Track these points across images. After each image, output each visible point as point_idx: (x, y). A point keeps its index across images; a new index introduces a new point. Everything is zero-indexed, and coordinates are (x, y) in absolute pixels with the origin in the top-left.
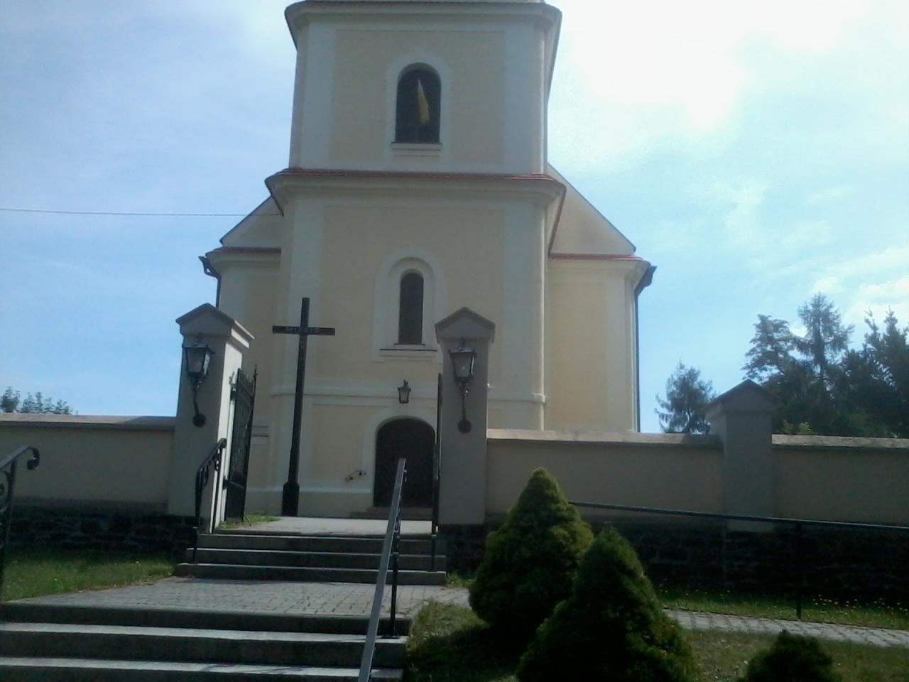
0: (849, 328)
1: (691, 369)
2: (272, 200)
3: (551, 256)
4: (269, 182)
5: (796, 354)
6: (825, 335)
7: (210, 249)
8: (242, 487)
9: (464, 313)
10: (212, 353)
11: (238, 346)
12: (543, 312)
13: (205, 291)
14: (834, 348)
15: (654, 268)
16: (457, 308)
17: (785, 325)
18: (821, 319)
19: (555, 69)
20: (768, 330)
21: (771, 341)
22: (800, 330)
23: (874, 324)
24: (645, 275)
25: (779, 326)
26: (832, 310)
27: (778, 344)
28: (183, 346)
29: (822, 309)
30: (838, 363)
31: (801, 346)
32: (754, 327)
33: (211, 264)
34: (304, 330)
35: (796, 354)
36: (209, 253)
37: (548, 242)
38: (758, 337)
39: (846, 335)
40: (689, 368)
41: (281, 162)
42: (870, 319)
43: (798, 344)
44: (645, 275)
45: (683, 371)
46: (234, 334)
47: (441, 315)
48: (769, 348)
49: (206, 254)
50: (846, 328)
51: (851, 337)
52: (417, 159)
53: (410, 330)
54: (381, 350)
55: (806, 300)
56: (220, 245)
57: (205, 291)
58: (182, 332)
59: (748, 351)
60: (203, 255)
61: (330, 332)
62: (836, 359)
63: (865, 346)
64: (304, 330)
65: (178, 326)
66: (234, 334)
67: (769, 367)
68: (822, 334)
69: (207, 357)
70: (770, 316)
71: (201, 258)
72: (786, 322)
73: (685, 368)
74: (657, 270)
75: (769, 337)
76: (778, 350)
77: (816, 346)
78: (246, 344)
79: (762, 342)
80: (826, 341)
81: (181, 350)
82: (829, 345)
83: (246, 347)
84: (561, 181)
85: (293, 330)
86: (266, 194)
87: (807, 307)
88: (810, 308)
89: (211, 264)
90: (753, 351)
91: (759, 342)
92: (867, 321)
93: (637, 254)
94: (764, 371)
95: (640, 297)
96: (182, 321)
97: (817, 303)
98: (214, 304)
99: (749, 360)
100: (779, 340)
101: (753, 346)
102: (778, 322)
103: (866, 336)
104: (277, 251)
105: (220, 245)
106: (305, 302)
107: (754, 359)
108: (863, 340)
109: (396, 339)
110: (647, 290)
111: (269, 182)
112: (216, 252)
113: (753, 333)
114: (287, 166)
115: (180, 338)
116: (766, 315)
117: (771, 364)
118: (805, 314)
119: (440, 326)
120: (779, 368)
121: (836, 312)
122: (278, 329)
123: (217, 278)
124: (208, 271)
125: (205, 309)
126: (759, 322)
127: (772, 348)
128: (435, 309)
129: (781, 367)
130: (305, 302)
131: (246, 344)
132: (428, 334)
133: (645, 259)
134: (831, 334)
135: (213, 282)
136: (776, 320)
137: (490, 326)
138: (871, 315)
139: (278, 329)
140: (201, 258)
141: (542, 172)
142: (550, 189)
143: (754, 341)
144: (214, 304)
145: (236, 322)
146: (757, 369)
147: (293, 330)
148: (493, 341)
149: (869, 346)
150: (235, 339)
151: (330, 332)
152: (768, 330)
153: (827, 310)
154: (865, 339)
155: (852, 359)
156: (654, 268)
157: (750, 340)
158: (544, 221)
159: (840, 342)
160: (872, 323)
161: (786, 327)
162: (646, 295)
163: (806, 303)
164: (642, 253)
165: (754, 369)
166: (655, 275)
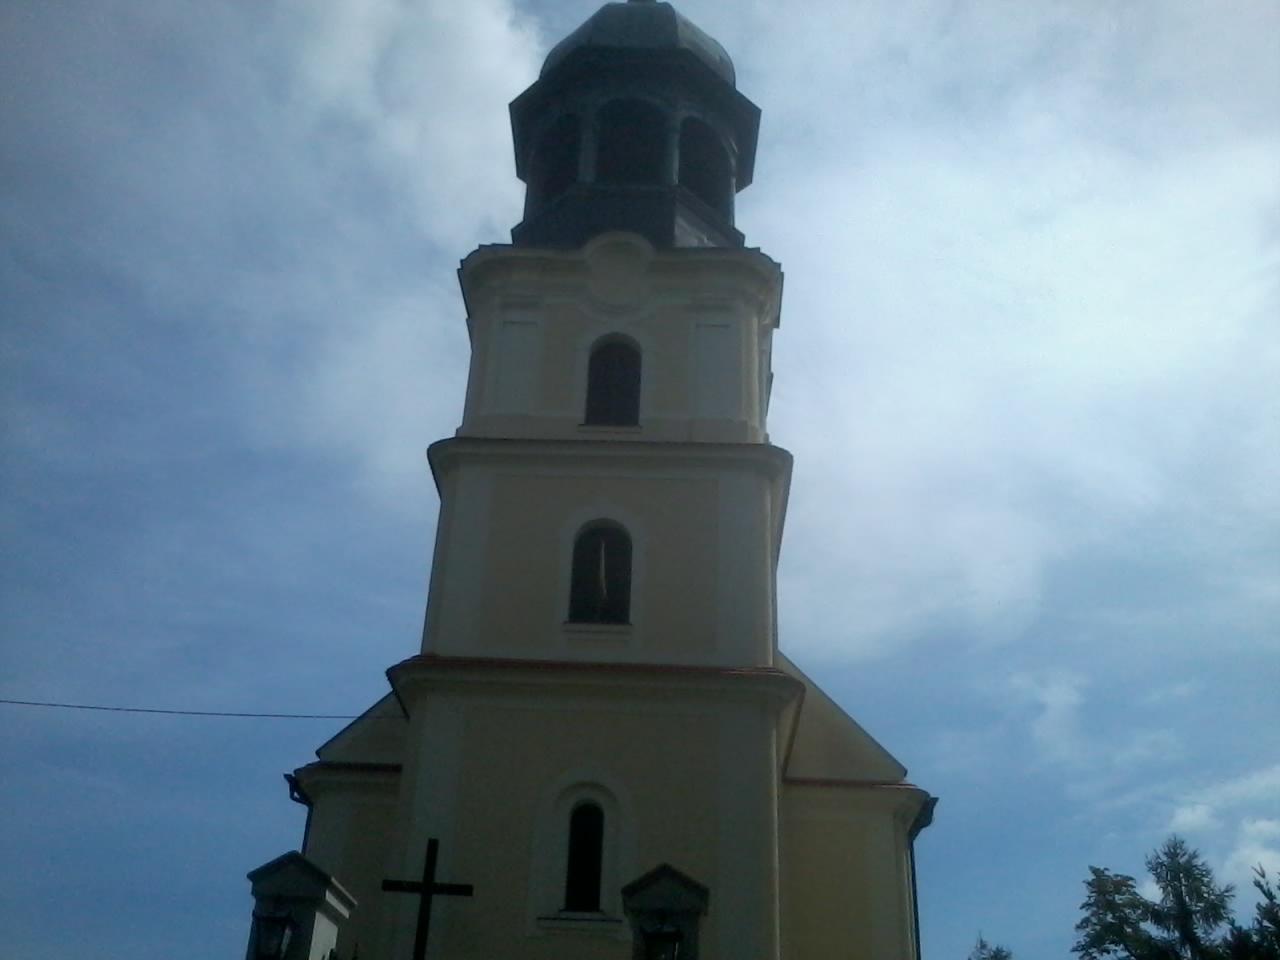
0: (1227, 891)
1: (997, 949)
2: (393, 699)
3: (787, 781)
4: (392, 674)
5: (1150, 928)
6: (1190, 899)
7: (301, 764)
8: (282, 955)
9: (665, 872)
10: (295, 927)
11: (334, 916)
12: (776, 865)
13: (285, 828)
14: (1206, 919)
15: (935, 800)
16: (652, 865)
17: (1130, 882)
18: (1181, 875)
19: (785, 527)
20: (1106, 890)
21: (1111, 906)
22: (1151, 892)
23: (1269, 890)
24: (923, 810)
25: (1123, 884)
26: (1198, 862)
27: (1123, 911)
28: (254, 914)
29: (1182, 860)
30: (1217, 943)
31: (1157, 915)
32: (1084, 885)
33: (301, 785)
34: (428, 888)
35: (1150, 928)
36: (299, 770)
37: (782, 758)
38: (1092, 900)
39: (1223, 901)
40: (994, 949)
41: (408, 645)
42: (1263, 882)
43: (1152, 913)
44: (923, 810)
45: (985, 952)
46: (330, 898)
47: (631, 876)
48: (1109, 918)
49: (295, 772)
50: (1223, 889)
51: (1232, 904)
52: (599, 645)
53: (582, 890)
54: (539, 919)
55: (1154, 844)
56: (317, 760)
57: (285, 828)
58: (255, 892)
59: (1078, 922)
60: (291, 773)
61: (465, 890)
62: (1212, 937)
63: (1260, 923)
64: (428, 888)
65: (250, 884)
66: (330, 898)
67: (1112, 947)
68: (1187, 899)
69: (288, 932)
70: (1106, 869)
71: (287, 777)
72: (1131, 879)
73: (989, 947)
74: (938, 804)
75: (1108, 900)
76: (1125, 920)
77: (1179, 917)
78: (345, 913)
79: (1098, 907)
80: (1194, 908)
81: (251, 919)
82: (1198, 915)
83: (344, 917)
84: (796, 676)
85: (411, 887)
86: (386, 688)
87: (1158, 857)
88: (1164, 858)
89: (301, 785)
90: (1085, 922)
91: (1095, 909)
92: (1258, 884)
93: (910, 779)
94: (1105, 954)
95: (916, 843)
96: (254, 876)
97: (1174, 849)
98: (300, 851)
99: (1081, 937)
100: (1124, 905)
101: (1085, 914)
102: (1119, 878)
103: (1259, 906)
104: (397, 769)
105: (317, 760)
106: (433, 846)
107: (1088, 935)
108: (1255, 913)
109: (562, 904)
110: (924, 833)
111: (392, 674)
112: (310, 769)
113: (1083, 894)
114: (418, 653)
115: (251, 903)
116: (1102, 868)
117: (1116, 943)
118: (1156, 868)
119: (630, 892)
120: (1127, 948)
121: (1203, 864)
122: (391, 886)
123: (308, 805)
124: (296, 794)
125: (291, 859)
126: (1091, 877)
127: (1114, 917)
128: (620, 866)
129: (1130, 948)
130: (433, 846)
131: (345, 913)
132: (610, 897)
133: (921, 787)
134: (1200, 898)
135: (302, 811)
136: (1117, 876)
137: (702, 893)
138: (1263, 876)
139: (391, 886)
140: (287, 777)
141: (771, 663)
142: (783, 689)
143: (1086, 906)
144: (300, 851)
145: (333, 880)
146: (1095, 950)
147: (411, 887)
148: (706, 914)
149: (1266, 923)
150: (328, 903)
151: (465, 890)
152: (1106, 890)
153: (1189, 861)
154: (1257, 911)
155: (1240, 939)
156: (935, 800)
157: (1080, 905)
158: (774, 733)
159: (1216, 910)
160: (1265, 887)
161: (1133, 887)
162: (925, 840)
163: (1155, 850)
164: (916, 778)
165: (1090, 951)
166: (937, 811)
